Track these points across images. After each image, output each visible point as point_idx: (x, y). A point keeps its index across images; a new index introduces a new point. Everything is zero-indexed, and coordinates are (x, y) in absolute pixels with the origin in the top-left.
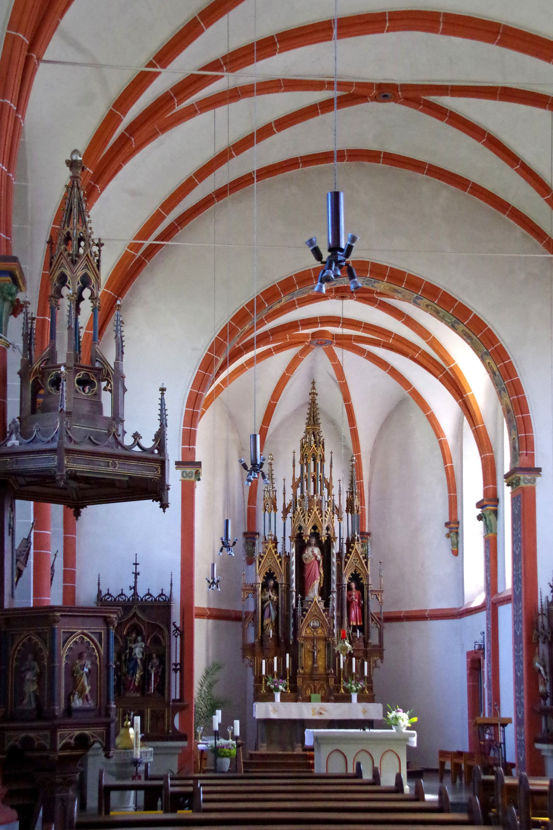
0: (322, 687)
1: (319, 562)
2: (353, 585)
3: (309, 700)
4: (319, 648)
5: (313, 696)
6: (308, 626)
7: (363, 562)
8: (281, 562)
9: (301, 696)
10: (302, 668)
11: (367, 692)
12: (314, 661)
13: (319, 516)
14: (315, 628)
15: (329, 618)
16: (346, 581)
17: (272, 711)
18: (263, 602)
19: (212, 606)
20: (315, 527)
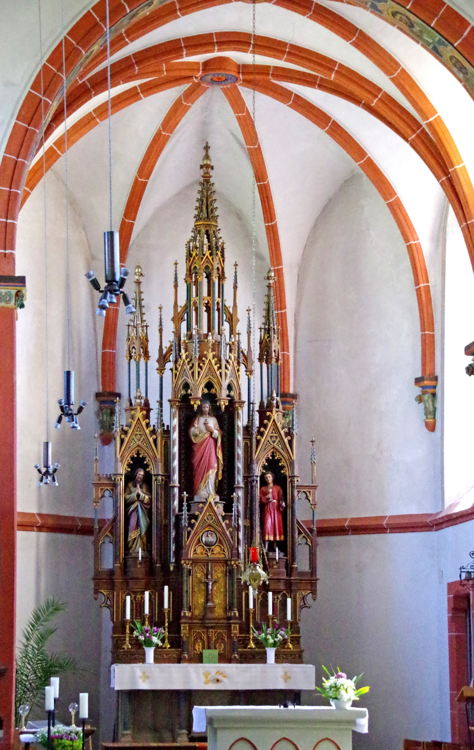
0: (220, 638)
1: (216, 440)
2: (270, 477)
3: (199, 659)
5: (206, 653)
6: (199, 541)
7: (286, 440)
8: (155, 441)
10: (190, 609)
13: (216, 368)
16: (258, 470)
18: (128, 504)
19: (44, 512)
20: (209, 385)
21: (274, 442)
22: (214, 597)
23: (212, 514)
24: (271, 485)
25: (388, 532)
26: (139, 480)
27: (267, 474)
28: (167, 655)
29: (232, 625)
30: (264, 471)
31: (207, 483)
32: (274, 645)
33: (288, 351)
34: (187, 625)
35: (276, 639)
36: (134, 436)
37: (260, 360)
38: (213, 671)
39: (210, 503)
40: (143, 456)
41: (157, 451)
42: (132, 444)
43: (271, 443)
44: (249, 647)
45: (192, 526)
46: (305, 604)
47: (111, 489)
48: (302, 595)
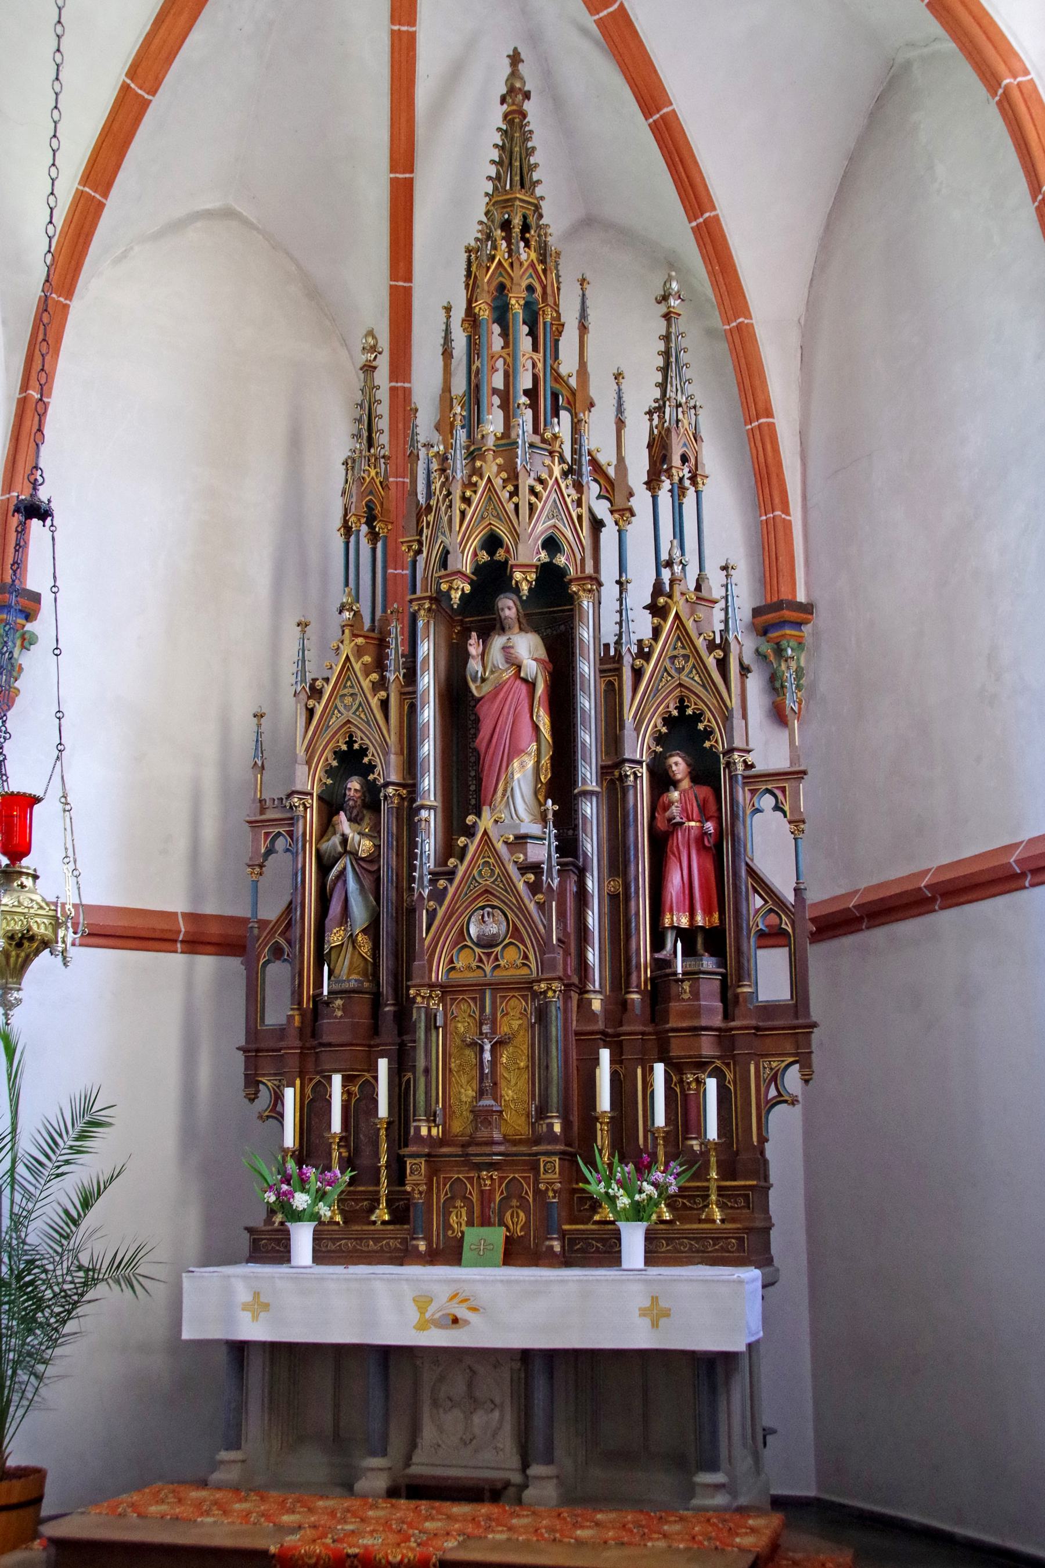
0: (513, 1192)
1: (532, 685)
2: (678, 766)
3: (450, 1253)
4: (504, 1029)
5: (473, 1236)
6: (463, 934)
7: (711, 661)
8: (385, 704)
9: (428, 1239)
10: (431, 1118)
11: (718, 1215)
12: (488, 1083)
14: (488, 943)
15: (540, 897)
16: (638, 747)
17: (246, 1307)
18: (324, 866)
19: (210, 908)
20: (492, 543)
21: (680, 670)
22: (503, 1084)
23: (492, 861)
24: (685, 784)
25: (1027, 884)
26: (351, 803)
27: (671, 756)
28: (376, 1240)
29: (409, 1162)
30: (659, 749)
31: (509, 793)
32: (637, 1212)
33: (786, 510)
34: (423, 1160)
35: (637, 1197)
36: (338, 702)
37: (652, 483)
38: (442, 1295)
39: (485, 832)
40: (361, 747)
41: (389, 731)
42: (334, 719)
43: (673, 672)
44: (597, 1218)
45: (439, 896)
46: (780, 1095)
47: (287, 832)
48: (771, 1069)
